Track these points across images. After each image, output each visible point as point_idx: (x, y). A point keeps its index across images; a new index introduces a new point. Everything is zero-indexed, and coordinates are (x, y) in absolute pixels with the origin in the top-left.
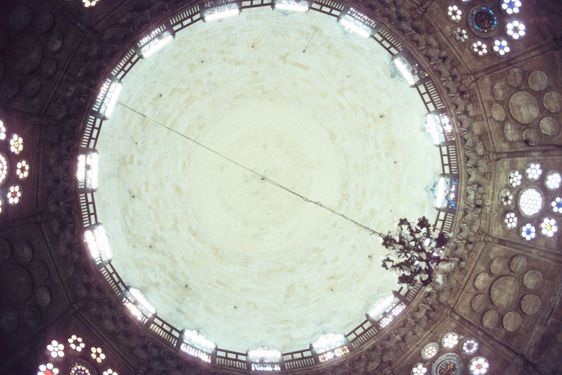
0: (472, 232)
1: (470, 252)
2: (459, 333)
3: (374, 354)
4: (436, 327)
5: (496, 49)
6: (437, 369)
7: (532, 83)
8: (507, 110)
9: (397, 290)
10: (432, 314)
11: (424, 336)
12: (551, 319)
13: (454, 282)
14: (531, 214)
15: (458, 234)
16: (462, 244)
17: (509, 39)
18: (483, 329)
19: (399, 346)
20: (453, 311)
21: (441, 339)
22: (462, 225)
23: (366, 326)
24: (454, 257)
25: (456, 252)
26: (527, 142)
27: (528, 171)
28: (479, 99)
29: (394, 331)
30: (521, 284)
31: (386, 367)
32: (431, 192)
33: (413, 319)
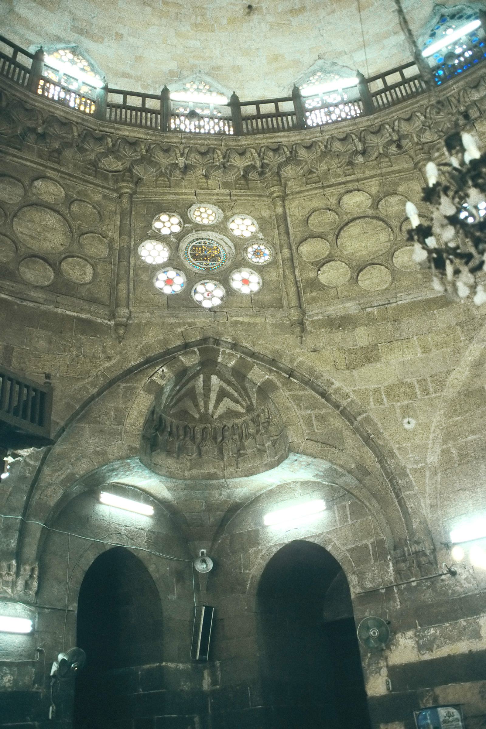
0: (419, 137)
1: (386, 155)
2: (262, 228)
3: (127, 151)
4: (241, 196)
6: (193, 241)
9: (241, 100)
10: (253, 175)
11: (215, 191)
12: (375, 310)
13: (324, 167)
15: (399, 119)
16: (388, 134)
18: (294, 252)
19: (171, 171)
20: (283, 198)
22: (418, 114)
23: (151, 104)
24: (360, 140)
25: (369, 137)
29: (185, 148)
30: (393, 250)
31: (127, 181)
32: (436, 20)
33: (224, 157)
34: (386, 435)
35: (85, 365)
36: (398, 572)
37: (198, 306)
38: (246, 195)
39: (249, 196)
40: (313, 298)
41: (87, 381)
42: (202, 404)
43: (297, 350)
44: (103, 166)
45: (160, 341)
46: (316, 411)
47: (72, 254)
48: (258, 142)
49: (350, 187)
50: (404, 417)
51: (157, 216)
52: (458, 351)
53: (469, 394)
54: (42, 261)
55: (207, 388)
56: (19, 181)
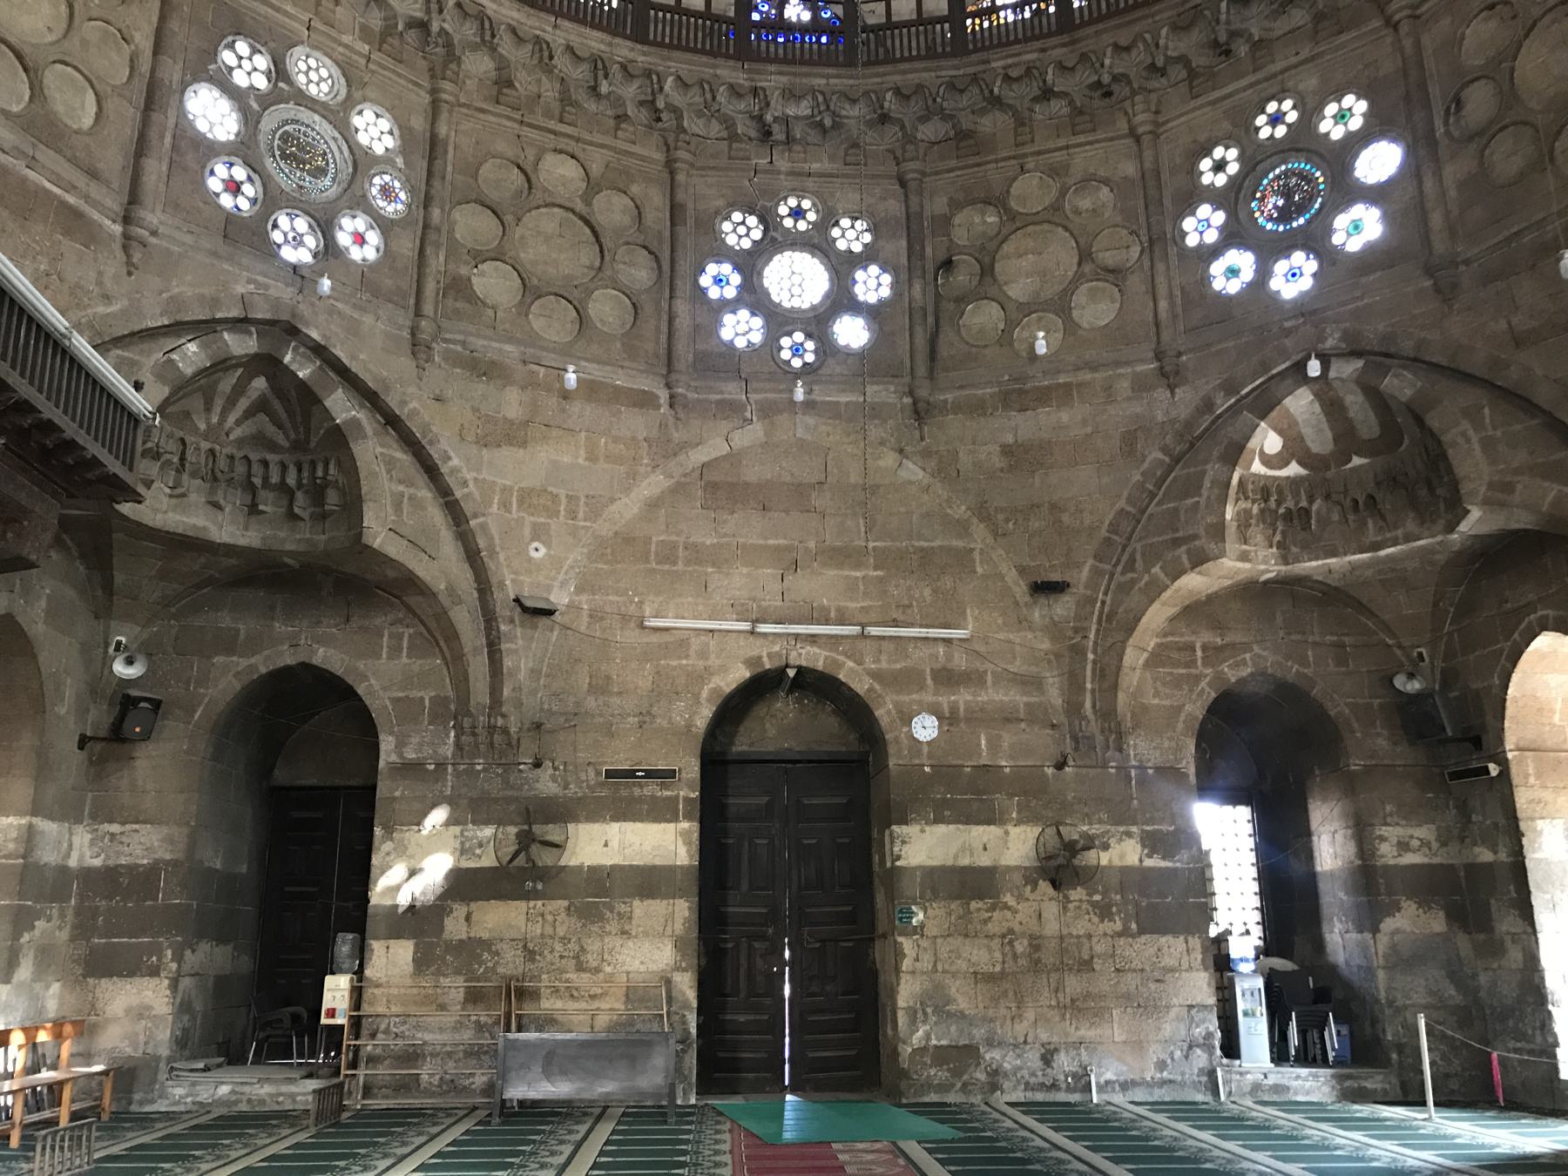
4: (385, 68)
5: (1204, 210)
7: (1091, 289)
8: (1036, 218)
11: (346, 39)
14: (766, 283)
17: (1215, 252)
21: (365, 100)
26: (947, 265)
27: (874, 269)
28: (1081, 139)
34: (502, 557)
36: (458, 746)
37: (269, 251)
38: (394, 71)
39: (399, 75)
40: (456, 311)
42: (217, 409)
43: (411, 390)
45: (201, 299)
46: (412, 490)
47: (67, 59)
49: (563, 143)
50: (533, 540)
51: (230, 39)
52: (633, 476)
53: (629, 540)
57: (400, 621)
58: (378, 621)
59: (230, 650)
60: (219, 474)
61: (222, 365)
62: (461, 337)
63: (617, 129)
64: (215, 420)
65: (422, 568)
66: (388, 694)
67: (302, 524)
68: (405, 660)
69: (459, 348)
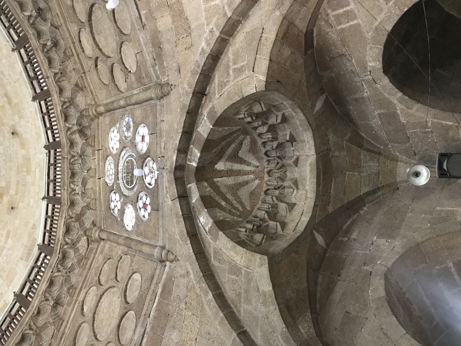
4: (99, 142)
35: (193, 298)
41: (203, 299)
42: (246, 178)
44: (84, 252)
46: (231, 64)
48: (63, 129)
49: (79, 50)
54: (123, 320)
55: (229, 173)
56: (80, 326)
57: (327, 21)
58: (334, 36)
59: (394, 116)
60: (279, 166)
61: (207, 202)
62: (151, 70)
63: (60, 26)
64: (252, 176)
65: (270, 36)
66: (384, 6)
67: (286, 114)
68: (352, 6)
69: (157, 68)
